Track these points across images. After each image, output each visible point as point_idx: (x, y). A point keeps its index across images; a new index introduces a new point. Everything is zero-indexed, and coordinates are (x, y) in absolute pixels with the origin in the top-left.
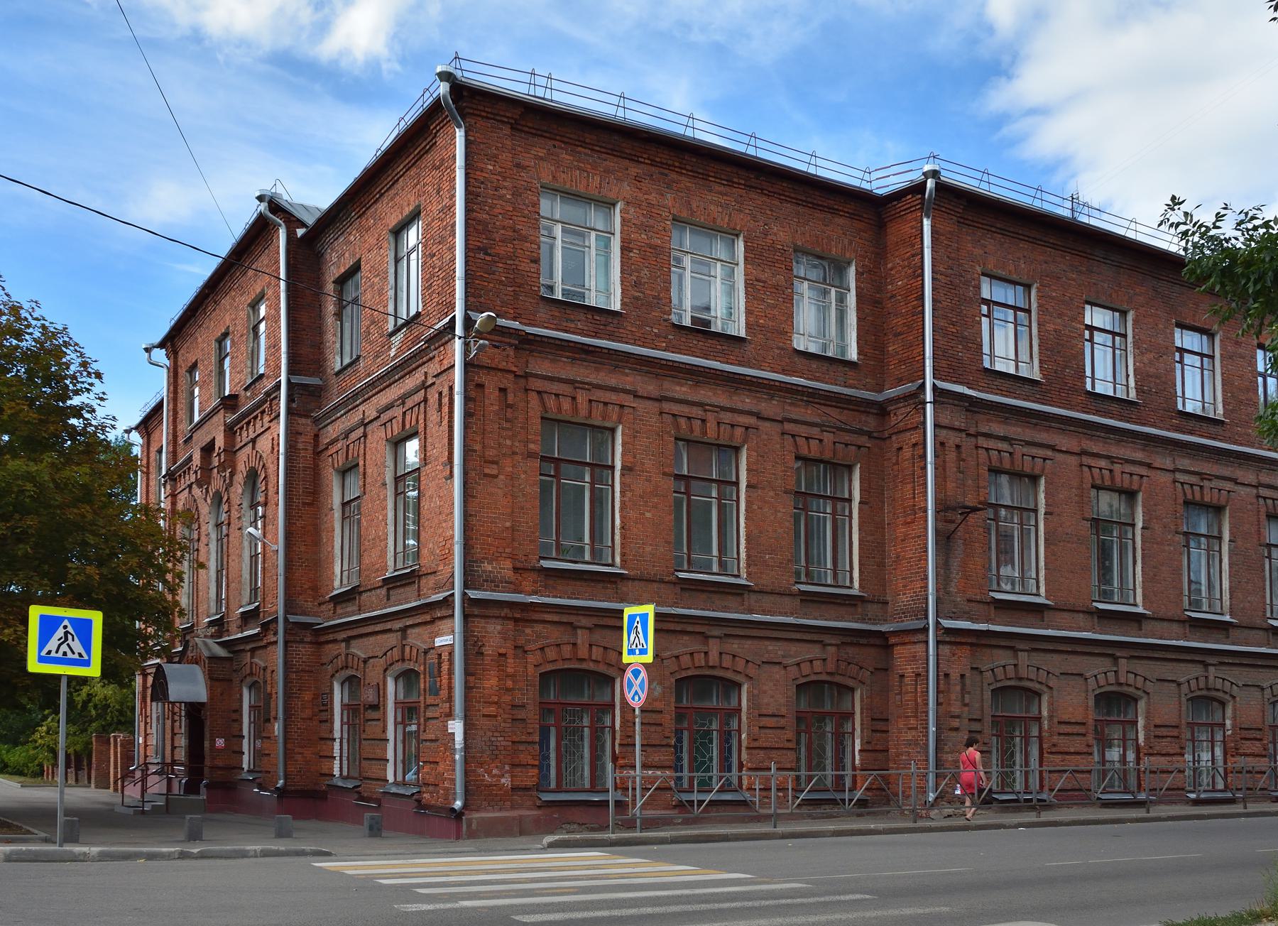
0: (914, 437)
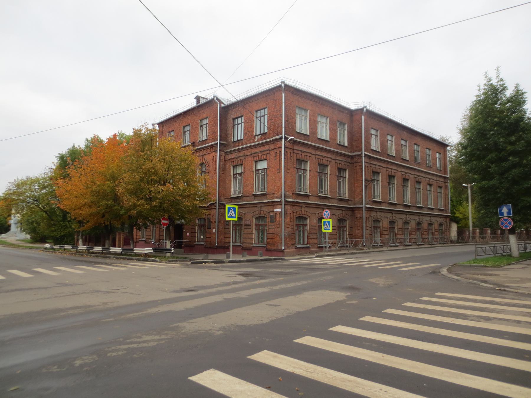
0: (360, 164)
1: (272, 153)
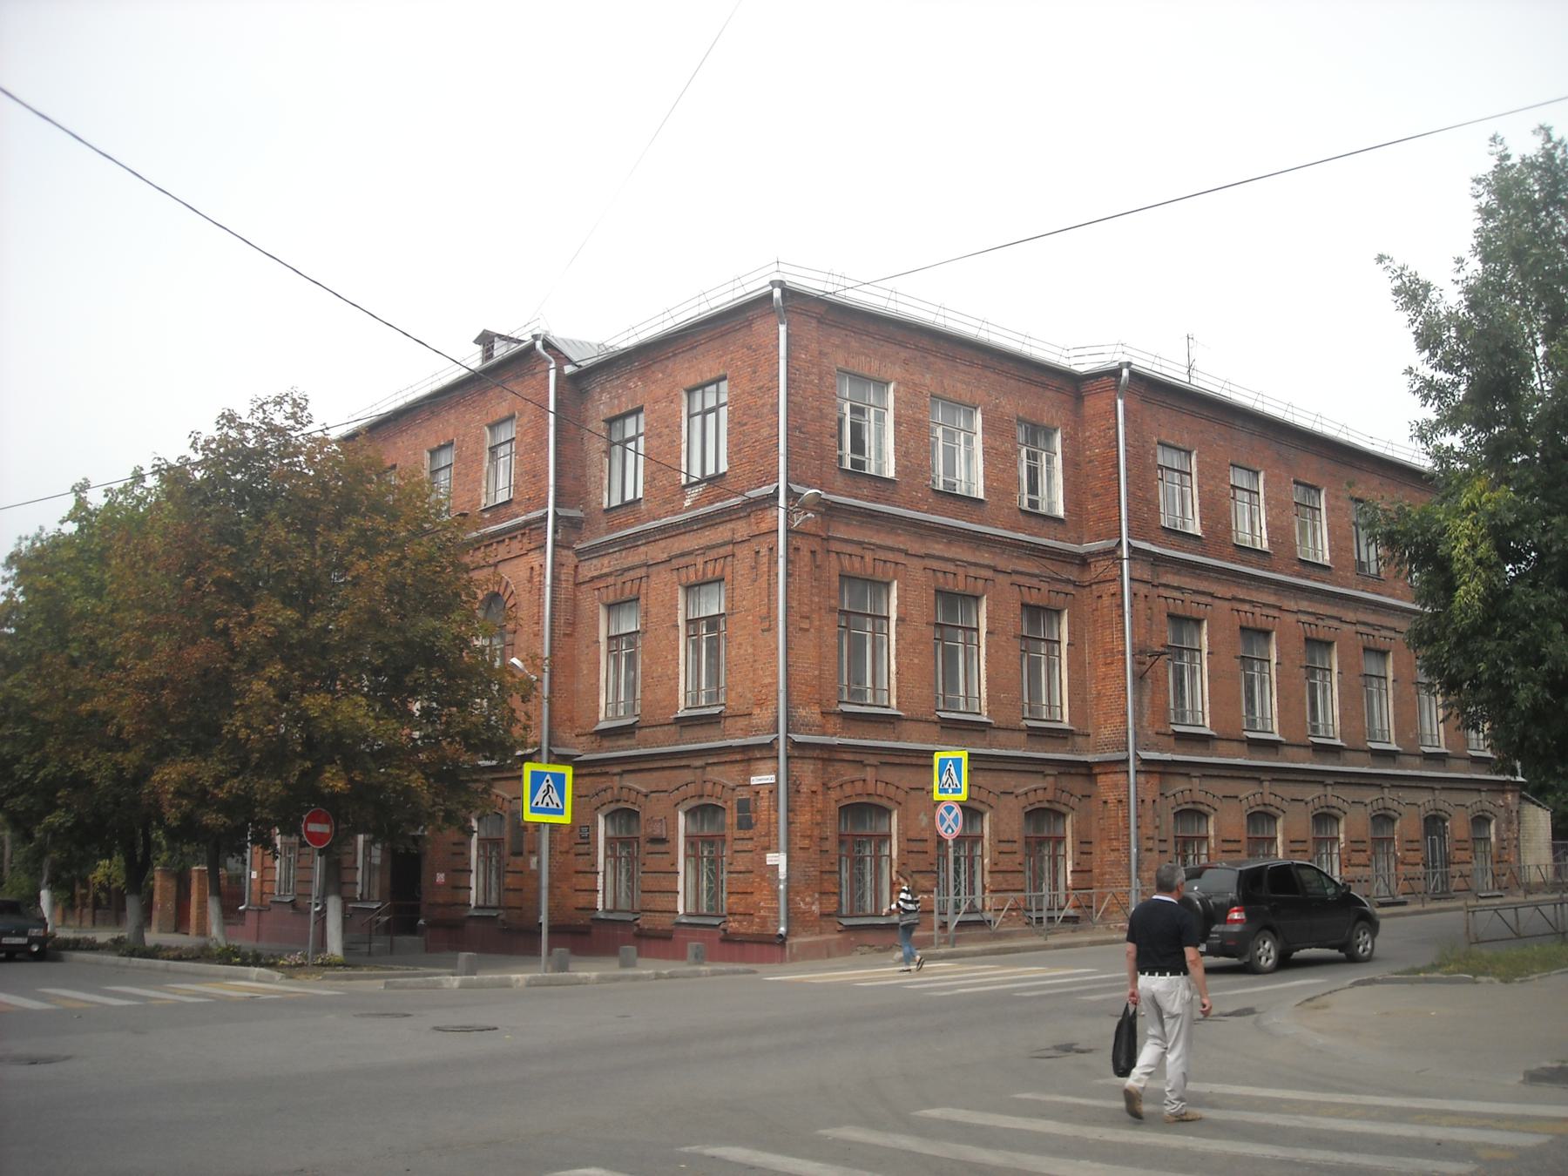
0: (1113, 588)
1: (744, 552)
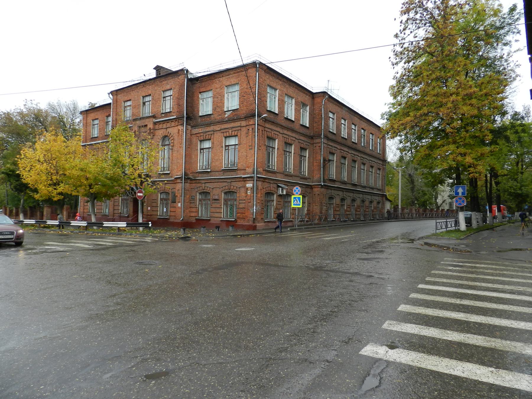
0: (319, 145)
1: (244, 130)
